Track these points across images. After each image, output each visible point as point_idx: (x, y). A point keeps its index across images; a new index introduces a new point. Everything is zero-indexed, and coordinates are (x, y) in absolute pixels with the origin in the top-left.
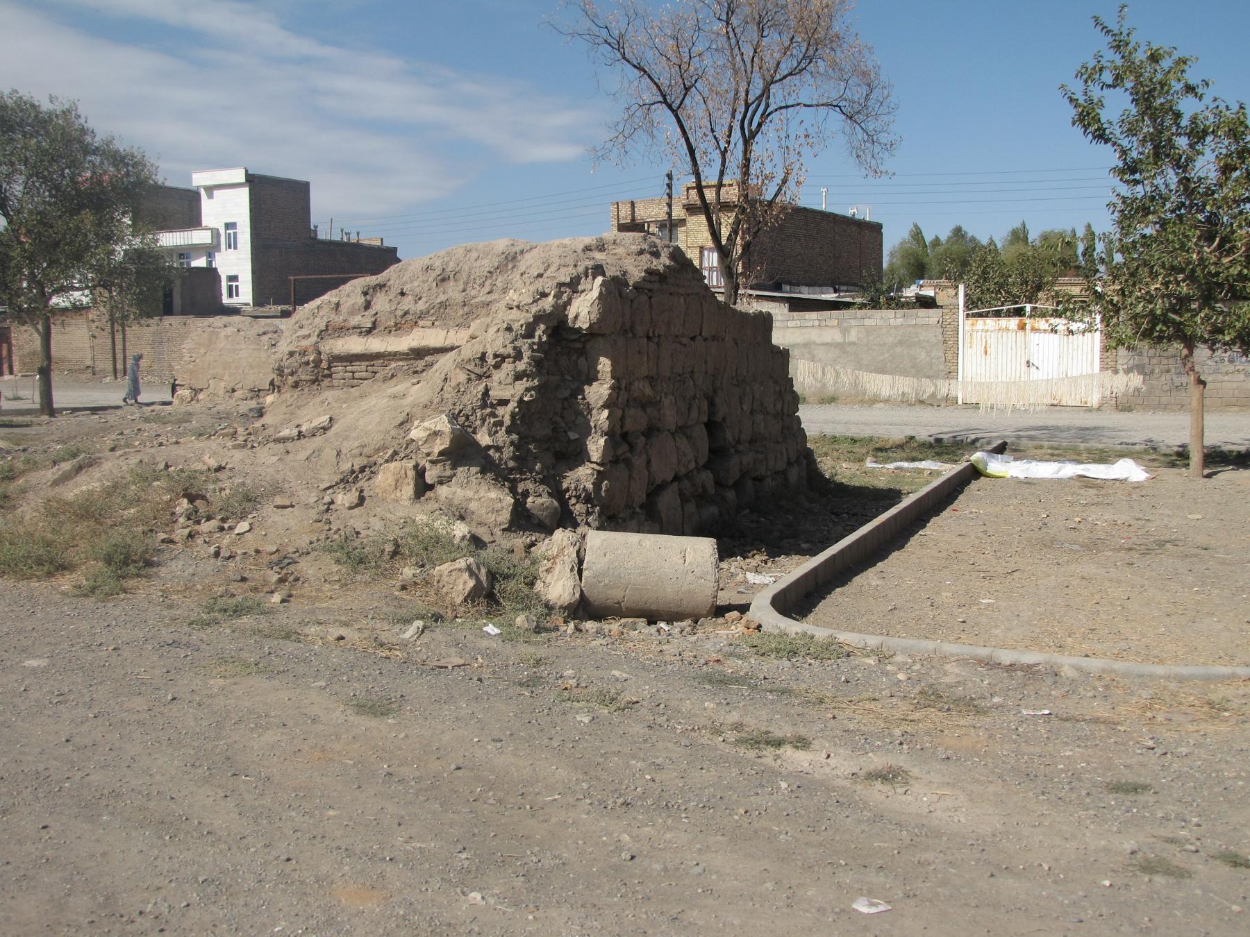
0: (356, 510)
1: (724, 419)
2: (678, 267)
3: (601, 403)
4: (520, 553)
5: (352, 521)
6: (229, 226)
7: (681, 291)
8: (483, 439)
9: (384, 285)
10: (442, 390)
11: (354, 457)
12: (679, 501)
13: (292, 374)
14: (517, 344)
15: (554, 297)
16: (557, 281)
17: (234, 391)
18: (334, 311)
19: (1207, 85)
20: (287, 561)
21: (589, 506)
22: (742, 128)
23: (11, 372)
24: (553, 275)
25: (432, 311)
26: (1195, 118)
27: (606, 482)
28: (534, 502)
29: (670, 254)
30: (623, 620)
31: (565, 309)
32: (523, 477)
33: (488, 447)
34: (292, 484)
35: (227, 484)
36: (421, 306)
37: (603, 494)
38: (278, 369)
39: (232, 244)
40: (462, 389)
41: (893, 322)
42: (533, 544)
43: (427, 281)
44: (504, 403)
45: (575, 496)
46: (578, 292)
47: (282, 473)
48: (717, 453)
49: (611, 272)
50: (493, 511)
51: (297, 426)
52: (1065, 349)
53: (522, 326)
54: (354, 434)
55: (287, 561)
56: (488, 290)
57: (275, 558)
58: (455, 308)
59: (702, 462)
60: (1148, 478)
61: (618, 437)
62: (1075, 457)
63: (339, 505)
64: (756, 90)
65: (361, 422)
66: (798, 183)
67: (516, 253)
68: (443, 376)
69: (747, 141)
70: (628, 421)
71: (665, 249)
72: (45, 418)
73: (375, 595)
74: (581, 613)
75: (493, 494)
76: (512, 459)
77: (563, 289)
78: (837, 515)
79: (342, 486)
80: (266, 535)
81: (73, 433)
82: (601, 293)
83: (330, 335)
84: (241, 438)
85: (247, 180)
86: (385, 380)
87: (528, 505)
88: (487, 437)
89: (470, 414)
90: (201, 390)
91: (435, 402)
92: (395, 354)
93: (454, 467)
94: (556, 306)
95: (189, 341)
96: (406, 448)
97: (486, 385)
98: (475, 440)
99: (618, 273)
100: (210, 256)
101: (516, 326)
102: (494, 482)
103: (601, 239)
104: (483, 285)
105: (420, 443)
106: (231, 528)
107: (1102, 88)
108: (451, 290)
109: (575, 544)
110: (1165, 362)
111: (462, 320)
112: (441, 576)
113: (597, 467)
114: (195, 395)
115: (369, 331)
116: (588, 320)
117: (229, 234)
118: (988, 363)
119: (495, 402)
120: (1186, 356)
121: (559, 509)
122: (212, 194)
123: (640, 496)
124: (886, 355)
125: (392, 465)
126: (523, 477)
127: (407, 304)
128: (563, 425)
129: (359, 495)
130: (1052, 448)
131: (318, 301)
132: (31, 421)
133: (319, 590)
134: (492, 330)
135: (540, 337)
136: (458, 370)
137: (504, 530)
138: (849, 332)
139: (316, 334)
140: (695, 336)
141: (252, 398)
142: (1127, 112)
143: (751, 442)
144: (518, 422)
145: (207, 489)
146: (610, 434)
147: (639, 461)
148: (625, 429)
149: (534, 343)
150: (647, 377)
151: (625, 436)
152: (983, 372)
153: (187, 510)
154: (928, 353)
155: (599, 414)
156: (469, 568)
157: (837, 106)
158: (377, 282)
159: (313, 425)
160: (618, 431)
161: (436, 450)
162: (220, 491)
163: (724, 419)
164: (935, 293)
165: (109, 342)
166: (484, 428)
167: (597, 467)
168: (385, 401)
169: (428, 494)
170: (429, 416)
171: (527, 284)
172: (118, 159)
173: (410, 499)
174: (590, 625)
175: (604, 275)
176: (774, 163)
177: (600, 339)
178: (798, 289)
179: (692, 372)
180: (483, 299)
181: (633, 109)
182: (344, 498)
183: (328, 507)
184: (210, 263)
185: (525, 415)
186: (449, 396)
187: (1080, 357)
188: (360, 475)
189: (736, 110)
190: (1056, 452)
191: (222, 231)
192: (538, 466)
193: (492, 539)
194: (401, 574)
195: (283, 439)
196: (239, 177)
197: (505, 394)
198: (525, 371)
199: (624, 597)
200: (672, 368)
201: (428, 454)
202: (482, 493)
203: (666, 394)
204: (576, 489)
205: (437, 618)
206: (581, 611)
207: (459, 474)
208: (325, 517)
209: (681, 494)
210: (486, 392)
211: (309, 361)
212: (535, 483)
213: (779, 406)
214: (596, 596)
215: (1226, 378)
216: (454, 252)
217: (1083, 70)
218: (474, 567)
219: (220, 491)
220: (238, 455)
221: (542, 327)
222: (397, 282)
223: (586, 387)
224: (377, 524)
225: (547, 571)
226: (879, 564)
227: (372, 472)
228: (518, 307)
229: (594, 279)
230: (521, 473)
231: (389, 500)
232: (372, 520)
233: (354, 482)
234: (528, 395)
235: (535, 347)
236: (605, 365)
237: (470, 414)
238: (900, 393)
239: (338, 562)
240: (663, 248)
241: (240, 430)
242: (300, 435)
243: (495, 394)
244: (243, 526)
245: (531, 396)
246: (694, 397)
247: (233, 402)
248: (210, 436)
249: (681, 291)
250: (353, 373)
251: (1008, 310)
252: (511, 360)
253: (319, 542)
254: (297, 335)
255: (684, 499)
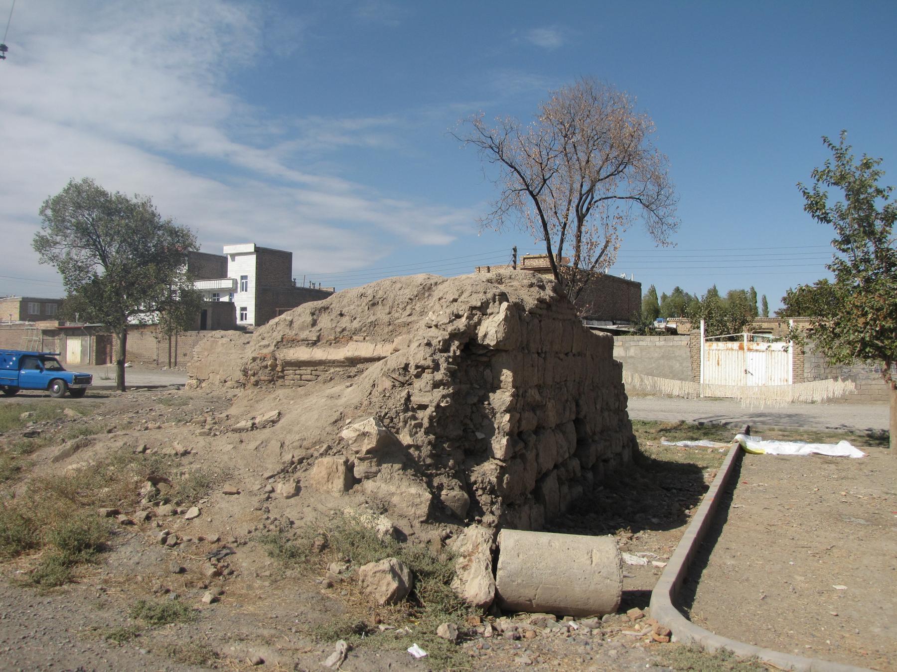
0: (292, 499)
1: (585, 417)
2: (559, 298)
3: (504, 408)
4: (437, 545)
5: (288, 510)
6: (244, 277)
7: (560, 317)
8: (405, 438)
9: (328, 308)
10: (370, 394)
11: (295, 448)
12: (557, 485)
13: (254, 375)
14: (436, 357)
15: (467, 318)
16: (469, 305)
17: (225, 382)
18: (288, 327)
19: (890, 189)
20: (225, 551)
21: (493, 496)
22: (577, 211)
23: (111, 362)
24: (466, 300)
25: (364, 329)
26: (888, 208)
27: (507, 475)
28: (447, 495)
29: (553, 287)
30: (535, 616)
31: (476, 329)
32: (439, 472)
33: (409, 446)
34: (241, 472)
35: (186, 469)
36: (356, 324)
37: (505, 486)
38: (244, 371)
39: (245, 288)
40: (388, 395)
41: (658, 344)
42: (448, 537)
43: (361, 305)
44: (423, 407)
45: (482, 488)
46: (486, 315)
47: (234, 460)
48: (582, 442)
49: (513, 299)
50: (413, 505)
51: (253, 419)
52: (770, 362)
53: (439, 342)
54: (296, 429)
55: (225, 551)
56: (408, 313)
57: (215, 547)
58: (382, 327)
59: (572, 451)
60: (865, 456)
61: (516, 436)
62: (799, 438)
63: (278, 494)
64: (585, 188)
65: (303, 418)
66: (615, 249)
67: (431, 285)
68: (371, 382)
69: (581, 219)
70: (524, 422)
71: (549, 284)
72: (119, 392)
73: (302, 596)
74: (495, 609)
75: (413, 490)
76: (429, 456)
77: (474, 312)
78: (668, 489)
79: (282, 475)
80: (211, 521)
81: (113, 409)
82: (506, 316)
83: (284, 345)
84: (207, 427)
85: (255, 251)
86: (325, 382)
87: (443, 497)
88: (408, 438)
89: (394, 417)
90: (204, 380)
91: (364, 404)
92: (334, 362)
93: (379, 464)
94: (468, 326)
95: (198, 346)
96: (339, 443)
97: (409, 392)
98: (398, 440)
99: (517, 300)
100: (231, 295)
101: (434, 342)
102: (413, 478)
103: (499, 274)
104: (404, 309)
105: (350, 442)
106: (183, 513)
107: (828, 185)
108: (379, 312)
109: (489, 541)
110: (834, 371)
111: (387, 337)
112: (366, 576)
113: (500, 463)
114: (200, 384)
115: (315, 343)
116: (495, 338)
117: (243, 282)
118: (720, 370)
119: (415, 407)
120: (886, 370)
121: (469, 501)
122: (234, 258)
123: (531, 484)
124: (654, 365)
125: (326, 460)
126: (439, 472)
127: (345, 322)
128: (472, 426)
129: (296, 486)
130: (780, 430)
131: (276, 319)
132: (110, 394)
133: (250, 587)
134: (414, 345)
135: (454, 352)
136: (384, 378)
137: (422, 522)
138: (629, 350)
139: (274, 344)
140: (568, 353)
141: (237, 387)
142: (839, 204)
143: (602, 432)
144: (435, 424)
145: (171, 472)
146: (509, 434)
147: (530, 455)
148: (520, 430)
149: (449, 357)
150: (536, 386)
151: (520, 434)
152: (717, 376)
153: (149, 492)
154: (681, 364)
155: (502, 417)
156: (392, 570)
157: (638, 199)
158: (322, 305)
159: (264, 418)
160: (516, 431)
161: (364, 449)
162: (181, 475)
163: (585, 417)
164: (677, 326)
165: (168, 345)
166: (406, 430)
167: (500, 463)
168: (323, 400)
169: (357, 487)
170: (360, 417)
171: (444, 307)
172: (174, 232)
173: (340, 492)
174: (503, 623)
175: (508, 301)
176: (598, 235)
177: (504, 354)
178: (591, 322)
179: (566, 380)
180: (404, 320)
181: (507, 194)
182: (283, 488)
183: (269, 495)
184: (231, 299)
185: (441, 416)
186: (376, 400)
187: (780, 367)
188: (298, 466)
189: (571, 200)
190: (786, 433)
191: (239, 281)
192: (451, 463)
193: (411, 532)
194: (329, 569)
195: (239, 429)
196: (251, 248)
197: (425, 400)
198: (441, 381)
199: (535, 595)
200: (554, 378)
201: (357, 452)
202: (403, 488)
203: (549, 398)
204: (482, 482)
205: (362, 629)
206: (495, 606)
207: (383, 471)
208: (265, 506)
209: (559, 479)
210: (408, 398)
211: (267, 365)
212: (448, 477)
213: (617, 404)
214: (510, 594)
215: (873, 382)
216: (383, 283)
217: (815, 172)
218: (397, 568)
219: (181, 475)
220: (202, 442)
221: (457, 343)
222: (337, 306)
223: (491, 394)
224: (310, 516)
225: (463, 568)
226: (720, 539)
227: (309, 464)
228: (436, 326)
229: (500, 304)
230: (437, 469)
231: (321, 491)
232: (306, 510)
233: (293, 472)
234: (445, 401)
235: (451, 360)
236: (507, 376)
237: (394, 417)
238: (686, 393)
239: (271, 554)
240: (547, 283)
241: (209, 419)
242: (254, 427)
243: (416, 399)
244: (193, 511)
245: (447, 402)
246: (567, 401)
247: (224, 389)
248: (187, 422)
249: (560, 317)
250: (301, 375)
251: (724, 338)
252: (430, 371)
253: (257, 532)
254: (260, 344)
255: (560, 482)
